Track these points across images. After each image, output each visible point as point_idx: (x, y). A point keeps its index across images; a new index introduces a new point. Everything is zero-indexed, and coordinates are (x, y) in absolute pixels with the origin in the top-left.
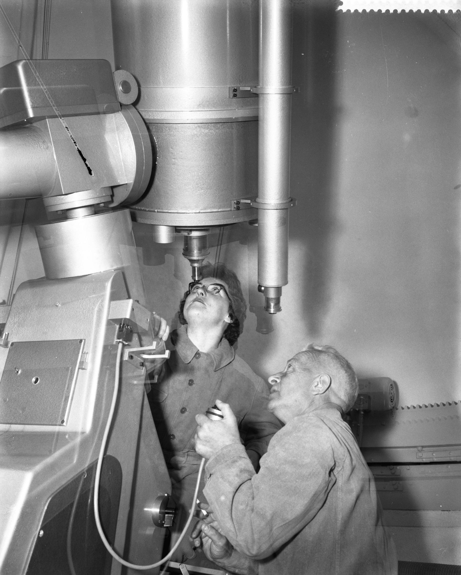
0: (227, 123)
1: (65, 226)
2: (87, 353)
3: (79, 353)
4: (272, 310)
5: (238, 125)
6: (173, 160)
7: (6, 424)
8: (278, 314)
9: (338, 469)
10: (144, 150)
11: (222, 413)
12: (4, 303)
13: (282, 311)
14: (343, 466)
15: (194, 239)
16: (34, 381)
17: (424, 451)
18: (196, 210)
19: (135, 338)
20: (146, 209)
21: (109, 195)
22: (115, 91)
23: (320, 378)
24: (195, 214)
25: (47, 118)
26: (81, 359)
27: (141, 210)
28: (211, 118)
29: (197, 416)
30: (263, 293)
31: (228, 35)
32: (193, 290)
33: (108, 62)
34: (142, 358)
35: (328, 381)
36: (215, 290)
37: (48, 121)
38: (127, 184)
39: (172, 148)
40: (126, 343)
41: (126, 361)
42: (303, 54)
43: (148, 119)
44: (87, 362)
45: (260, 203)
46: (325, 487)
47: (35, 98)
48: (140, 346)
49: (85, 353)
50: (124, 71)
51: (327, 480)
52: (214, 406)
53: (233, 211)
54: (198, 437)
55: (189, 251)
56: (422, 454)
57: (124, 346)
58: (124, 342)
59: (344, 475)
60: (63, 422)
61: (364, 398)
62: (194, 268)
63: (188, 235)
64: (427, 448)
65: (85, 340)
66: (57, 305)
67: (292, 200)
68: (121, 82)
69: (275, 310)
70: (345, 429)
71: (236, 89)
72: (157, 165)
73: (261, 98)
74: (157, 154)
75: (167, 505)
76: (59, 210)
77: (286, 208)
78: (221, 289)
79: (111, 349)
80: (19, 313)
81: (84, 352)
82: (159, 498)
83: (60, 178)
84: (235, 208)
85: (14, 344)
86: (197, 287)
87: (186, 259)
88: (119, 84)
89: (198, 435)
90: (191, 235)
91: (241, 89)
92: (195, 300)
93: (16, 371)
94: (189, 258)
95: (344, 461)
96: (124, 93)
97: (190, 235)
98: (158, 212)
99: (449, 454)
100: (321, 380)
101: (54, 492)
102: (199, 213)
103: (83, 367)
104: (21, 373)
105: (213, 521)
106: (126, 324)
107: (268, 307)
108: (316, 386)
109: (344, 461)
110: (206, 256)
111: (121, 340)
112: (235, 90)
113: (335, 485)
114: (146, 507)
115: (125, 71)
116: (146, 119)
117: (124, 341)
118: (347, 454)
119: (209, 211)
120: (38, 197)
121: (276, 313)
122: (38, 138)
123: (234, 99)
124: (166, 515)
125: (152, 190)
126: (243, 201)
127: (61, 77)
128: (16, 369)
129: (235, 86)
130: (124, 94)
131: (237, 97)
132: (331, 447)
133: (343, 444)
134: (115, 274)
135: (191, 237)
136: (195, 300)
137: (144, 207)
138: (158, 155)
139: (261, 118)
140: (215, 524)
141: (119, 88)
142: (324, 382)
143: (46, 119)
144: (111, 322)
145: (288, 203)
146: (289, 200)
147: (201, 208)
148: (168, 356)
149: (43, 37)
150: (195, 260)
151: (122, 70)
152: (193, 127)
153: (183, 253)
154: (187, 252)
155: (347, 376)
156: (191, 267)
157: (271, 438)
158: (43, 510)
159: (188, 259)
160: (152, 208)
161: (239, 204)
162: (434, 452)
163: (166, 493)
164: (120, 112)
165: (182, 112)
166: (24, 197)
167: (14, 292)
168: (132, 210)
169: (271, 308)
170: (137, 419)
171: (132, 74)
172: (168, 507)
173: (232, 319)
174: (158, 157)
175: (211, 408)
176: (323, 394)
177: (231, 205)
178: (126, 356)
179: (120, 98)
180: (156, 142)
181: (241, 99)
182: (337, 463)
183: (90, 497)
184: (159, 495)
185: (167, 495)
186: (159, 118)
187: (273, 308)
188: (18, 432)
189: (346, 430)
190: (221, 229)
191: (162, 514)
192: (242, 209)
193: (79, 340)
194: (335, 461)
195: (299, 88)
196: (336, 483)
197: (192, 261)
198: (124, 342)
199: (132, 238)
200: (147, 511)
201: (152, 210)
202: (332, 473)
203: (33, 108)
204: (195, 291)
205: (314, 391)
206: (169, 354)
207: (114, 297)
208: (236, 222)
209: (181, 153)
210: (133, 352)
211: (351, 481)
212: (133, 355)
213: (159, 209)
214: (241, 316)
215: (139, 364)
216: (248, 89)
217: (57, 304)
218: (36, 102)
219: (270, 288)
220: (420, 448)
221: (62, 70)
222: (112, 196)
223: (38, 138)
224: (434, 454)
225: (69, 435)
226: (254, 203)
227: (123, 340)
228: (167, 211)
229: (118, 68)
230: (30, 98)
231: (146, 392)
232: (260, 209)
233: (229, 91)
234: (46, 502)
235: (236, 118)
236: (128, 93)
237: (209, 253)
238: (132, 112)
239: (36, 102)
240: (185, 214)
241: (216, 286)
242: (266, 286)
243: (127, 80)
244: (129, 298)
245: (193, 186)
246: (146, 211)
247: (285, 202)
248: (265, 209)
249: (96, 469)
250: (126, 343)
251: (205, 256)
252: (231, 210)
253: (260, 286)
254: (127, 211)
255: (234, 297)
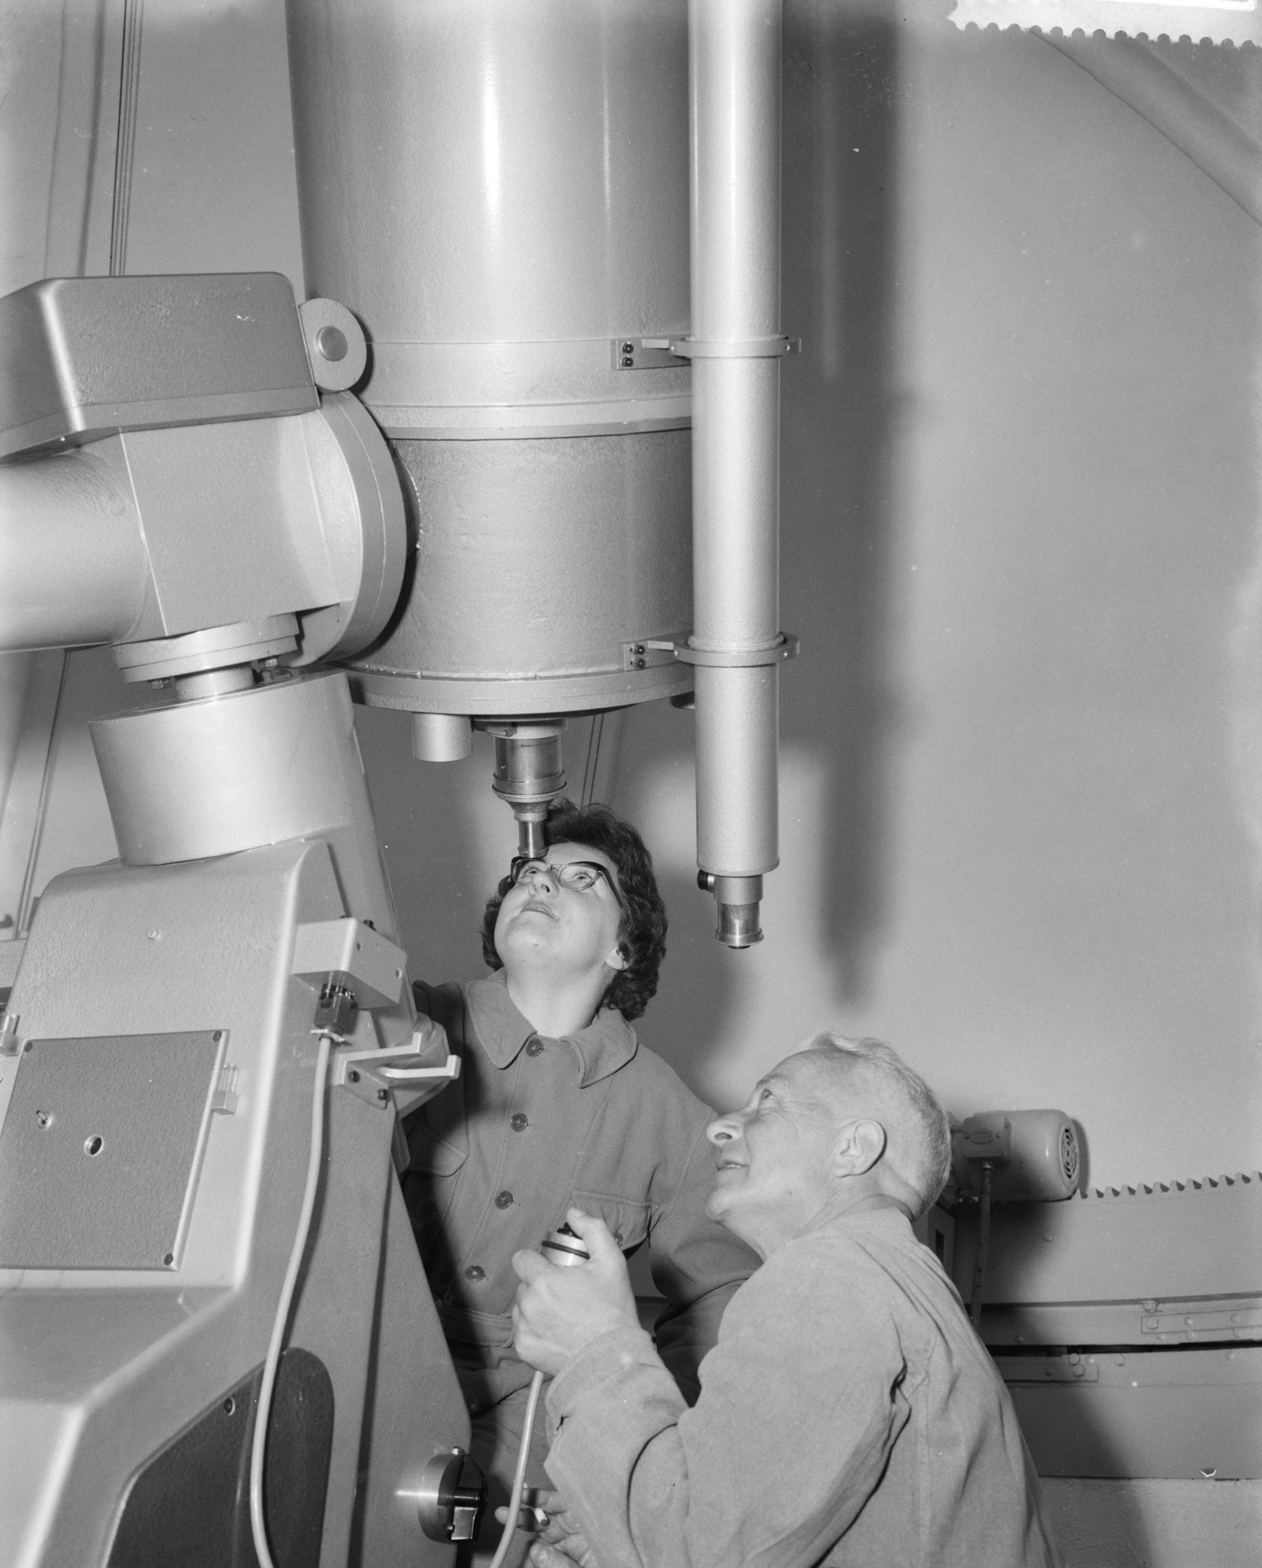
0: (609, 438)
1: (171, 720)
2: (234, 1069)
3: (212, 1069)
4: (737, 938)
5: (638, 442)
6: (464, 537)
7: (10, 1267)
8: (755, 947)
9: (914, 1381)
10: (385, 514)
11: (586, 1245)
12: (8, 922)
13: (762, 941)
14: (927, 1372)
15: (523, 746)
16: (89, 1147)
17: (1161, 1311)
18: (527, 672)
19: (365, 1022)
20: (393, 669)
21: (289, 634)
22: (305, 355)
23: (856, 1130)
24: (523, 682)
25: (122, 432)
26: (218, 1083)
27: (378, 672)
28: (566, 424)
29: (517, 1255)
30: (711, 892)
31: (608, 201)
32: (523, 877)
33: (288, 280)
34: (384, 1076)
35: (876, 1138)
36: (581, 878)
37: (125, 439)
38: (338, 604)
39: (459, 506)
40: (341, 1039)
41: (341, 1086)
42: (857, 150)
43: (393, 428)
44: (234, 1094)
45: (699, 651)
46: (884, 1432)
47: (90, 380)
48: (377, 1045)
49: (228, 1067)
50: (327, 300)
51: (887, 1412)
52: (562, 1227)
53: (628, 671)
54: (521, 1313)
55: (510, 779)
56: (1158, 1322)
57: (334, 1045)
58: (335, 1036)
59: (930, 1397)
60: (169, 1259)
61: (993, 1169)
62: (524, 826)
63: (506, 738)
64: (1171, 1304)
65: (228, 1031)
66: (153, 936)
67: (785, 641)
68: (320, 331)
69: (743, 938)
70: (925, 1267)
71: (630, 346)
72: (420, 551)
73: (697, 367)
74: (419, 522)
75: (458, 1481)
76: (155, 677)
77: (768, 662)
78: (600, 875)
79: (298, 1056)
80: (47, 959)
81: (225, 1066)
82: (437, 1460)
83: (157, 591)
84: (631, 663)
85: (35, 1046)
86: (533, 868)
87: (501, 800)
88: (315, 337)
89: (520, 1307)
90: (514, 737)
91: (643, 347)
92: (527, 907)
93: (40, 1120)
94: (510, 800)
95: (930, 1358)
96: (328, 359)
97: (511, 738)
98: (423, 677)
99: (1231, 1320)
100: (857, 1136)
101: (145, 1461)
102: (535, 678)
103: (224, 1107)
104: (53, 1126)
105: (566, 1535)
106: (340, 987)
107: (725, 928)
108: (843, 1153)
109: (930, 1358)
110: (555, 793)
111: (326, 1031)
112: (628, 349)
113: (908, 1426)
114: (401, 1488)
115: (331, 302)
116: (389, 428)
117: (336, 1032)
118: (935, 1338)
119: (562, 672)
120: (99, 643)
121: (748, 946)
122: (97, 485)
123: (626, 372)
124: (457, 1509)
125: (408, 618)
126: (653, 645)
127: (158, 323)
128: (41, 1114)
129: (627, 336)
130: (327, 361)
131: (634, 366)
132: (891, 1321)
133: (923, 1312)
134: (308, 848)
135: (513, 741)
136: (527, 907)
137: (386, 665)
138: (421, 525)
139: (696, 424)
140: (573, 1543)
141: (316, 348)
142: (866, 1142)
143: (119, 433)
144: (297, 981)
145: (773, 649)
146: (777, 640)
147: (539, 665)
148: (455, 1072)
149: (114, 212)
150: (526, 804)
151: (322, 299)
152: (517, 449)
153: (493, 787)
154: (505, 781)
155: (924, 1126)
156: (516, 824)
157: (724, 1304)
158: (115, 1510)
159: (507, 801)
160: (407, 667)
161: (641, 653)
162: (1189, 1314)
163: (455, 1447)
164: (318, 411)
165: (484, 409)
166: (63, 644)
167: (37, 890)
168: (354, 674)
169: (734, 934)
170: (375, 1244)
171: (347, 308)
172: (461, 1485)
173: (626, 959)
174: (421, 531)
175: (556, 1233)
176: (862, 1176)
177: (621, 654)
178: (341, 1074)
179: (316, 375)
180: (416, 489)
181: (643, 371)
182: (909, 1364)
183: (240, 1484)
184: (436, 1452)
185: (459, 1452)
186: (423, 426)
187: (740, 934)
188: (48, 1290)
189: (929, 1270)
190: (596, 720)
191: (449, 1505)
192: (651, 667)
193: (213, 1034)
194: (904, 1359)
195: (800, 340)
196: (912, 1418)
197: (519, 807)
198: (335, 1036)
199: (354, 747)
200: (404, 1499)
201: (407, 671)
202: (898, 1392)
203: (85, 406)
204: (527, 880)
205: (839, 1166)
206: (456, 1066)
207: (308, 912)
208: (636, 702)
209: (485, 518)
210: (359, 1063)
211: (953, 1414)
212: (358, 1070)
213: (427, 669)
214: (652, 948)
215: (377, 1095)
216: (664, 344)
217: (152, 933)
218: (91, 390)
219: (731, 879)
220: (1150, 1305)
221: (161, 303)
222: (300, 638)
223: (97, 485)
224: (1190, 1322)
225: (186, 1297)
226: (684, 651)
227: (331, 1031)
228: (447, 675)
229: (312, 294)
230: (76, 379)
231: (397, 1170)
232: (701, 666)
233: (613, 350)
234: (124, 1487)
235: (630, 423)
236: (337, 360)
237: (566, 783)
238: (351, 409)
239: (91, 390)
240: (498, 682)
241: (584, 869)
242: (720, 874)
243: (337, 326)
244: (348, 914)
245: (516, 607)
246: (391, 674)
247: (766, 646)
248: (713, 667)
249: (258, 1393)
250: (341, 1039)
251: (552, 794)
252: (620, 671)
253: (703, 874)
254: (339, 679)
255: (633, 899)
